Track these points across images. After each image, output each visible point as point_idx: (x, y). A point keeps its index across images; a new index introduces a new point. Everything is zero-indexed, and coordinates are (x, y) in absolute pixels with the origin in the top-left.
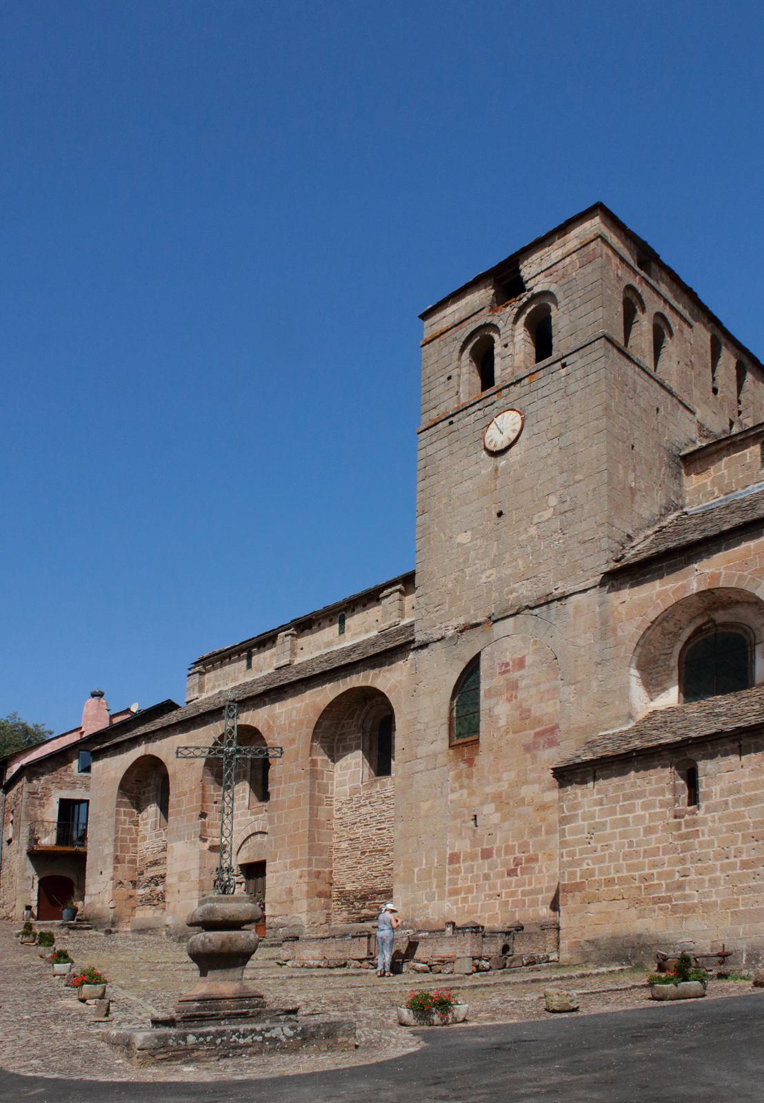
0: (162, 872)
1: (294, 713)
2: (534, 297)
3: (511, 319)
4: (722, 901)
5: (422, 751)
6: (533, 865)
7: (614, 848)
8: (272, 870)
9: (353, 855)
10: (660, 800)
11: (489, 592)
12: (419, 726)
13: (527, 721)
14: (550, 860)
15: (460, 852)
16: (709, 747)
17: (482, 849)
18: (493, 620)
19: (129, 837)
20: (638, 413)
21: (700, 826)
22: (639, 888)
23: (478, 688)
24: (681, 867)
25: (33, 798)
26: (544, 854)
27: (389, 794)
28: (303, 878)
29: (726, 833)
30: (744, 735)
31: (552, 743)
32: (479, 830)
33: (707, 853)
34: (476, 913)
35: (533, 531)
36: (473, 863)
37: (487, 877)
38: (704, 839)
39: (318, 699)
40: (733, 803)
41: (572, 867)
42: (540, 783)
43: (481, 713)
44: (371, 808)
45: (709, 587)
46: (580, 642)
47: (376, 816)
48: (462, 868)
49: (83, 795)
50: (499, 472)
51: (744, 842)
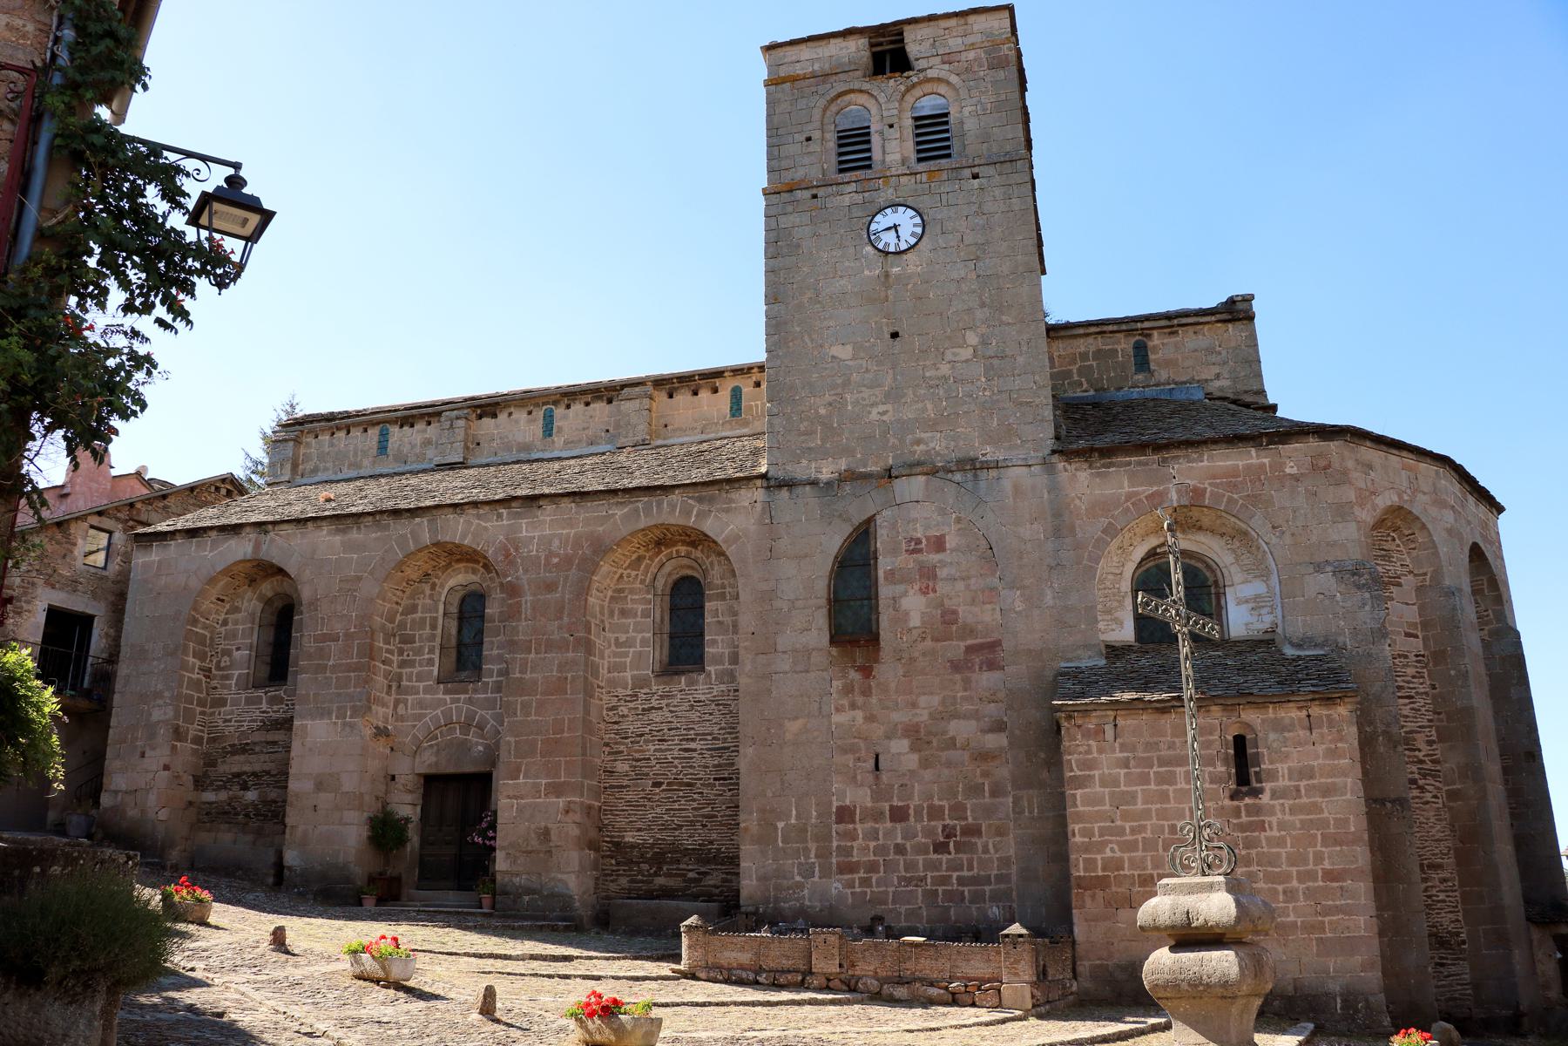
1: (556, 543)
4: (1302, 922)
7: (1149, 832)
8: (511, 793)
10: (1210, 773)
13: (954, 628)
15: (855, 806)
21: (1265, 815)
27: (702, 698)
28: (571, 814)
29: (1300, 829)
30: (1317, 703)
31: (992, 666)
34: (886, 903)
36: (877, 826)
37: (900, 850)
39: (601, 529)
40: (1306, 790)
41: (1090, 853)
42: (978, 719)
44: (669, 715)
47: (678, 728)
48: (860, 832)
50: (891, 280)
51: (1324, 844)
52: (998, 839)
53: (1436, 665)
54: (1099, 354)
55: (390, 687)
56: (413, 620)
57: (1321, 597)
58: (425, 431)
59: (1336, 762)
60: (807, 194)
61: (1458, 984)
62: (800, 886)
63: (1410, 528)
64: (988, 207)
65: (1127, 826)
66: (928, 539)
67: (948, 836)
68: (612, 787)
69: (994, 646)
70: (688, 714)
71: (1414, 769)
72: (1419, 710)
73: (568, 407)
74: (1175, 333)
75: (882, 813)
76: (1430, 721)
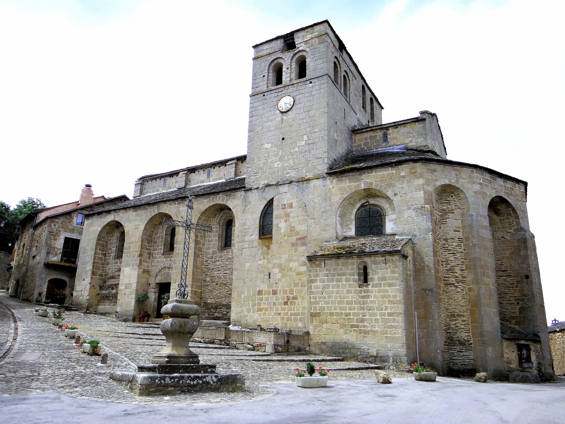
0: (116, 283)
2: (300, 51)
3: (290, 58)
4: (380, 330)
5: (247, 238)
6: (295, 301)
9: (211, 285)
10: (353, 278)
11: (278, 171)
12: (245, 227)
13: (293, 232)
14: (303, 299)
16: (373, 257)
17: (273, 290)
18: (278, 185)
19: (100, 262)
20: (338, 109)
22: (345, 319)
23: (272, 213)
24: (362, 311)
25: (51, 235)
26: (300, 296)
27: (230, 257)
30: (387, 254)
31: (304, 244)
32: (271, 280)
33: (373, 306)
35: (297, 149)
37: (274, 304)
38: (372, 299)
43: (274, 225)
44: (221, 262)
45: (368, 187)
46: (317, 201)
49: (77, 237)
53: (466, 241)
54: (371, 137)
55: (150, 257)
56: (157, 236)
57: (409, 218)
58: (176, 178)
59: (394, 275)
60: (262, 95)
61: (467, 359)
62: (247, 316)
63: (457, 192)
64: (314, 93)
67: (288, 300)
68: (205, 285)
69: (304, 238)
70: (226, 262)
71: (454, 279)
72: (458, 258)
73: (214, 168)
74: (398, 127)
76: (462, 262)
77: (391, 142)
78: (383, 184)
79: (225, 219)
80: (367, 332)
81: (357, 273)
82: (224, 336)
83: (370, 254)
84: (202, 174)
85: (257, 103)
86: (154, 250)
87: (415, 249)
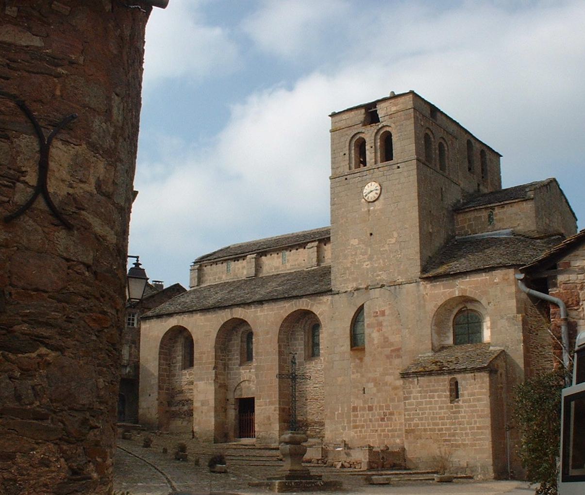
2: (384, 127)
6: (392, 417)
10: (445, 395)
12: (335, 337)
13: (387, 343)
17: (368, 406)
22: (438, 434)
27: (319, 369)
31: (399, 356)
52: (399, 416)
62: (342, 433)
65: (420, 412)
66: (380, 311)
69: (399, 350)
73: (290, 251)
74: (504, 207)
75: (413, 404)
77: (499, 225)
78: (477, 292)
79: (310, 324)
80: (458, 446)
81: (449, 389)
82: (320, 455)
83: (460, 371)
84: (276, 258)
85: (339, 188)
86: (229, 359)
87: (508, 360)
